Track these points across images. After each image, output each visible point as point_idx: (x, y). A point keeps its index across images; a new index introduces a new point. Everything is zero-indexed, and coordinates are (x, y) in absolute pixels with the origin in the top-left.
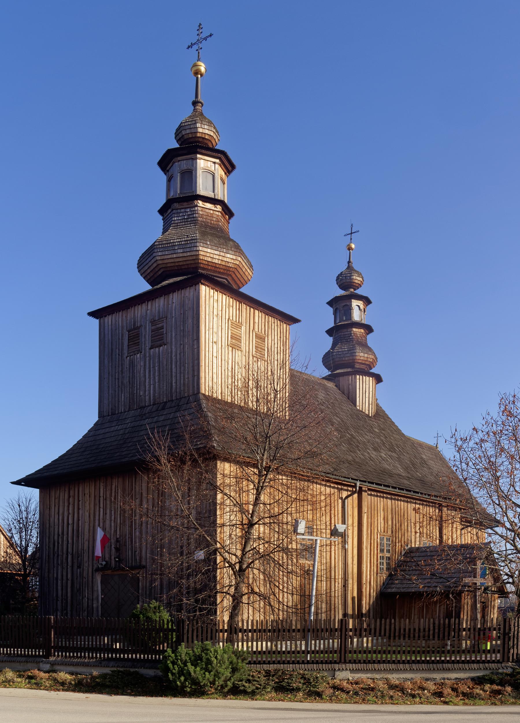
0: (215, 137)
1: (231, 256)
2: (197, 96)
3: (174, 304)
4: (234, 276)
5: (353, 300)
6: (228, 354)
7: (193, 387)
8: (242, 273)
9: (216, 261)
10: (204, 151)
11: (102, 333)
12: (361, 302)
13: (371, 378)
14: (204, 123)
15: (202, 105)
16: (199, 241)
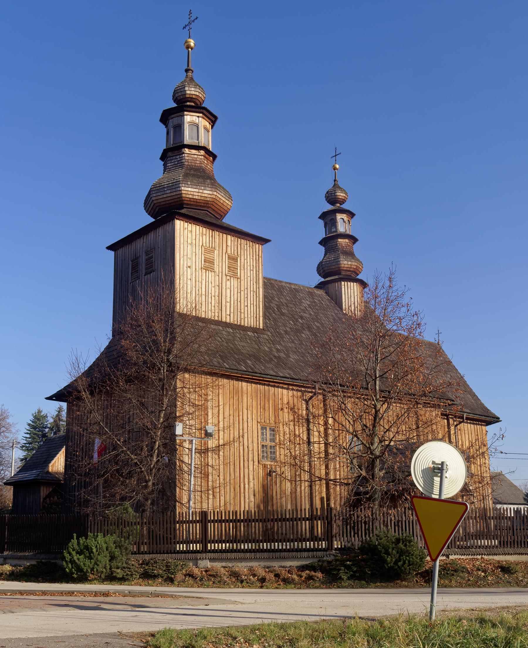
0: (200, 95)
1: (208, 192)
2: (188, 66)
4: (213, 207)
5: (337, 214)
6: (203, 275)
8: (220, 204)
9: (197, 197)
10: (189, 109)
12: (345, 215)
13: (355, 284)
14: (191, 86)
15: (193, 72)
16: (181, 182)
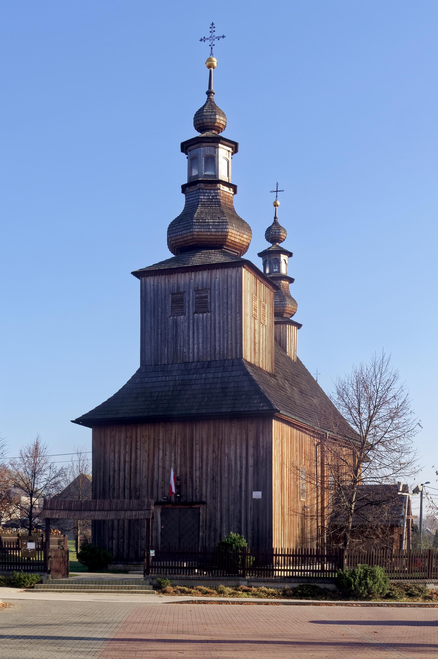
3: (218, 279)
7: (236, 352)
11: (144, 291)
